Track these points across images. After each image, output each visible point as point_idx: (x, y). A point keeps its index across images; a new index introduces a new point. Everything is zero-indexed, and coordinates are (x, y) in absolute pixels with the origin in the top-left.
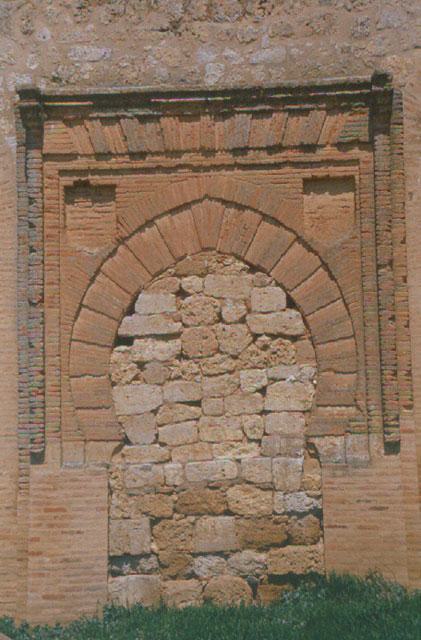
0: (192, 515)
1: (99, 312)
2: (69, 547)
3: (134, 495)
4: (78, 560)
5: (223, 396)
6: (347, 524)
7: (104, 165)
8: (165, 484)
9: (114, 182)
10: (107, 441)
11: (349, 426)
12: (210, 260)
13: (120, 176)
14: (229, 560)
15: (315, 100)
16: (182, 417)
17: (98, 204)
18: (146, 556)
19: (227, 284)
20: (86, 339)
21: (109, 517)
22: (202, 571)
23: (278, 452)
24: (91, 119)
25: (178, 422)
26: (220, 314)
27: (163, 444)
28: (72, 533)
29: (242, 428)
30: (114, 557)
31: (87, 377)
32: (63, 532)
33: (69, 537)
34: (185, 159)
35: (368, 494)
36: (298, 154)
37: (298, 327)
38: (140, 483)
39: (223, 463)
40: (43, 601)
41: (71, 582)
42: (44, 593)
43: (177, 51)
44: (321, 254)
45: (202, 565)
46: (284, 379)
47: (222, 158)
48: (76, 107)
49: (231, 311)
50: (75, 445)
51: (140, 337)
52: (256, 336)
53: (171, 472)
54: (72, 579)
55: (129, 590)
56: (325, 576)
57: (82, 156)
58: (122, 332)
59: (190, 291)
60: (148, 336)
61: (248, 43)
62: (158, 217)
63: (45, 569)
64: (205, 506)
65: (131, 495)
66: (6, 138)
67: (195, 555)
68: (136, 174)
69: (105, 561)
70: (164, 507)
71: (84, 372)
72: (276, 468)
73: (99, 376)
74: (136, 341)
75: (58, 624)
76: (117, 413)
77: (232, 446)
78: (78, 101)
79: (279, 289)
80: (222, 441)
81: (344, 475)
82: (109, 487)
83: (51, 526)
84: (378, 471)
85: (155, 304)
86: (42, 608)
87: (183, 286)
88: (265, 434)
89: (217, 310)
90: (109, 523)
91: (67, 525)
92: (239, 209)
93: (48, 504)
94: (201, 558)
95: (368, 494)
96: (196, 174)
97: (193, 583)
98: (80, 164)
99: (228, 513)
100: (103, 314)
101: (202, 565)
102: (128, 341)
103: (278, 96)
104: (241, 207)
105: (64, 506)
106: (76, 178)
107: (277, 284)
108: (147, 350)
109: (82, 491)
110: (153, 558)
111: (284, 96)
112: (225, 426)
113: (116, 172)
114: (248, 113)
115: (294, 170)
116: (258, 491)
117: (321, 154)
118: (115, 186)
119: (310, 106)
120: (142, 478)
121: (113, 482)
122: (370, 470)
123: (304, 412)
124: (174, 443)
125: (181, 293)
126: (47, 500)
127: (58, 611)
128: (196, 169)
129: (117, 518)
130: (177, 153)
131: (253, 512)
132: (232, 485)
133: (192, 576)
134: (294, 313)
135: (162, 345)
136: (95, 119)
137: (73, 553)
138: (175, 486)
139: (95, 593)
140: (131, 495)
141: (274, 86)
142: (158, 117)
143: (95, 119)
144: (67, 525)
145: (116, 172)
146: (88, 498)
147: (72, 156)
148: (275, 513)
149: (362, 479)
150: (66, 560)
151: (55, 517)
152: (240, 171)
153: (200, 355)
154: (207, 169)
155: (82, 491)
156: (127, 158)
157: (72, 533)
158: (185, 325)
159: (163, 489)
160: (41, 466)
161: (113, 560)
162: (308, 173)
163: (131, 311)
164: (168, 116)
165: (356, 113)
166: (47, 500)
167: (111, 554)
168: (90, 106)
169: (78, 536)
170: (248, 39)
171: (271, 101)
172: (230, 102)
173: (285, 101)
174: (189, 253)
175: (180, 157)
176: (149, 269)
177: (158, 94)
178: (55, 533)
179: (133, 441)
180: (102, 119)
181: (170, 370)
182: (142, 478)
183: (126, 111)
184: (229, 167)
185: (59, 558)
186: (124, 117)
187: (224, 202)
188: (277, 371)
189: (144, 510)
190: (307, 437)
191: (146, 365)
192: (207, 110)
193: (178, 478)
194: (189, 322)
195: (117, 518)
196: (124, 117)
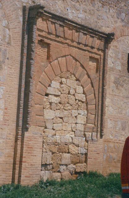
0: (61, 152)
1: (42, 84)
2: (32, 160)
3: (49, 145)
4: (34, 165)
5: (68, 117)
6: (92, 158)
7: (49, 36)
8: (56, 143)
9: (50, 43)
10: (42, 127)
11: (93, 130)
12: (68, 74)
13: (52, 42)
14: (67, 167)
15: (96, 35)
16: (59, 122)
17: (42, 48)
18: (49, 165)
19: (71, 82)
20: (39, 92)
21: (43, 151)
22: (62, 170)
23: (78, 135)
24: (49, 21)
25: (58, 123)
26: (69, 92)
27: (54, 130)
28: (33, 156)
29: (72, 127)
30: (43, 164)
31: (38, 105)
32: (31, 155)
33: (33, 157)
34: (67, 41)
35: (96, 149)
36: (90, 49)
37: (84, 100)
38: (51, 141)
39: (68, 137)
40: (25, 178)
41: (32, 172)
42: (25, 175)
43: (63, 5)
44: (92, 79)
45: (62, 168)
46: (81, 114)
47: (75, 44)
48: (47, 15)
49: (72, 92)
50: (35, 127)
51: (51, 94)
52: (76, 100)
53: (58, 138)
54: (32, 171)
55: (46, 175)
56: (87, 172)
57: (45, 32)
58: (48, 92)
59: (63, 83)
60: (53, 95)
61: (78, 10)
62: (59, 57)
63: (26, 167)
64: (64, 150)
65: (48, 145)
66: (20, 17)
67: (60, 165)
68: (82, 50)
69: (40, 166)
70: (55, 150)
71: (38, 103)
72: (80, 140)
73: (41, 105)
74: (50, 96)
75: (28, 185)
76: (45, 118)
77: (69, 132)
78: (48, 14)
79: (82, 87)
80: (67, 130)
81: (92, 144)
82: (43, 141)
83: (29, 153)
84: (99, 143)
85: (55, 84)
86: (25, 180)
87: (62, 81)
88: (76, 130)
89: (69, 90)
90: (42, 153)
91: (32, 153)
92: (76, 61)
93: (28, 145)
94: (61, 166)
95: (96, 149)
96: (68, 47)
97: (59, 174)
98: (43, 34)
99: (69, 153)
100: (44, 85)
101: (62, 168)
102: (47, 95)
103: (90, 31)
104: (76, 60)
105: (32, 147)
106: (41, 38)
107: (81, 86)
108: (54, 99)
109: (36, 142)
110: (51, 166)
111: (99, 34)
112: (68, 126)
113: (51, 39)
114: (82, 33)
115: (88, 53)
116: (75, 147)
117: (95, 50)
118: (50, 44)
119: (95, 36)
120: (51, 140)
121: (44, 140)
122: (97, 143)
123: (84, 124)
124: (57, 130)
125: (61, 83)
126: (28, 144)
127: (28, 181)
128: (69, 45)
129: (44, 152)
130: (66, 39)
131: (74, 153)
132: (70, 144)
133: (59, 172)
134: (84, 95)
135: (56, 98)
136: (50, 21)
137: (33, 163)
138: (58, 143)
139: (37, 176)
140: (48, 145)
141: (91, 28)
142: (64, 26)
143: (50, 21)
144: (32, 153)
145: (51, 39)
146: (38, 145)
147: (42, 31)
148: (78, 154)
149: (95, 145)
150: (32, 165)
151: (30, 150)
152: (77, 49)
153: (64, 103)
154: (71, 46)
155: (36, 142)
156: (55, 36)
157: (33, 156)
158: (61, 93)
159: (55, 144)
160: (27, 132)
161: (42, 165)
162: (91, 55)
163: (50, 86)
164: (66, 27)
165: (102, 41)
166: (28, 144)
167: (42, 164)
168: (51, 17)
169: (35, 157)
170: (78, 9)
171: (89, 32)
172: (79, 28)
173: (91, 33)
174: (64, 71)
175: (66, 40)
176: (56, 73)
177: (67, 20)
178: (29, 156)
179: (48, 127)
180: (51, 22)
181: (57, 106)
182: (51, 140)
183: (57, 21)
184: (76, 47)
185: (30, 164)
186: (57, 23)
187: (73, 57)
188: (80, 111)
189: (51, 150)
190: (84, 131)
191: (52, 104)
192: (97, 37)
193: (59, 140)
194: (62, 92)
195: (44, 152)
196: (57, 23)
